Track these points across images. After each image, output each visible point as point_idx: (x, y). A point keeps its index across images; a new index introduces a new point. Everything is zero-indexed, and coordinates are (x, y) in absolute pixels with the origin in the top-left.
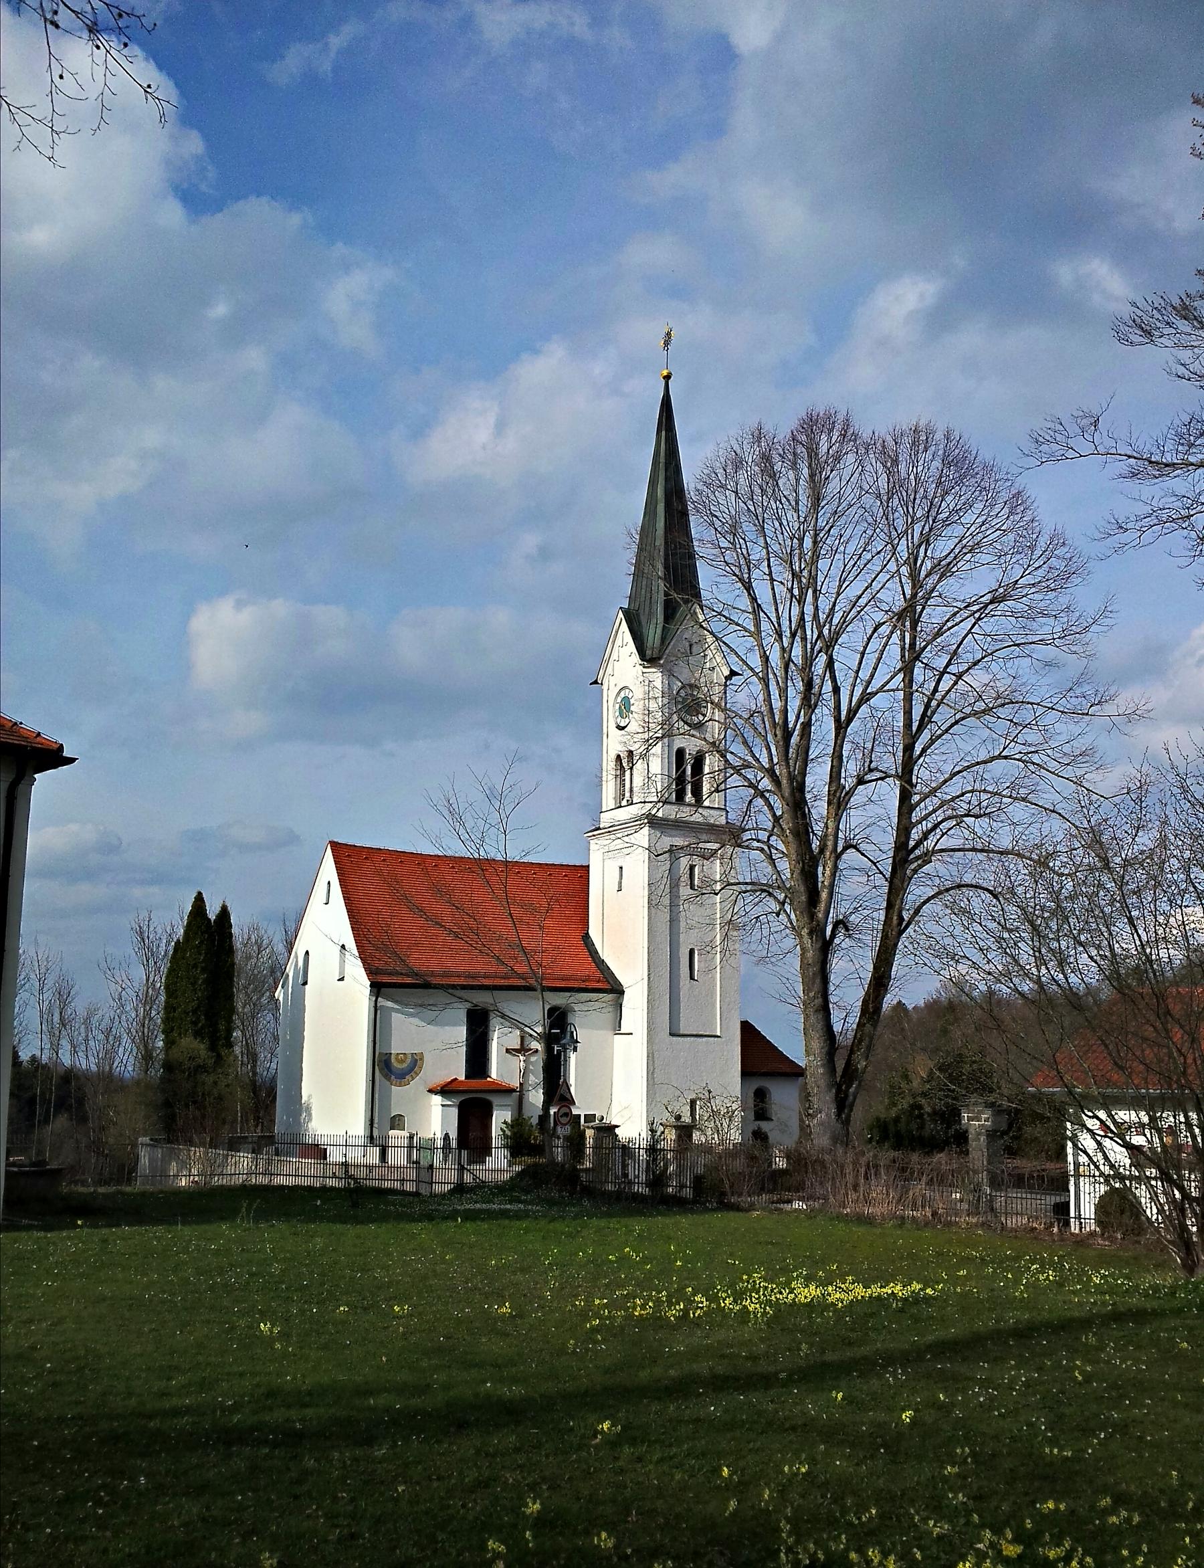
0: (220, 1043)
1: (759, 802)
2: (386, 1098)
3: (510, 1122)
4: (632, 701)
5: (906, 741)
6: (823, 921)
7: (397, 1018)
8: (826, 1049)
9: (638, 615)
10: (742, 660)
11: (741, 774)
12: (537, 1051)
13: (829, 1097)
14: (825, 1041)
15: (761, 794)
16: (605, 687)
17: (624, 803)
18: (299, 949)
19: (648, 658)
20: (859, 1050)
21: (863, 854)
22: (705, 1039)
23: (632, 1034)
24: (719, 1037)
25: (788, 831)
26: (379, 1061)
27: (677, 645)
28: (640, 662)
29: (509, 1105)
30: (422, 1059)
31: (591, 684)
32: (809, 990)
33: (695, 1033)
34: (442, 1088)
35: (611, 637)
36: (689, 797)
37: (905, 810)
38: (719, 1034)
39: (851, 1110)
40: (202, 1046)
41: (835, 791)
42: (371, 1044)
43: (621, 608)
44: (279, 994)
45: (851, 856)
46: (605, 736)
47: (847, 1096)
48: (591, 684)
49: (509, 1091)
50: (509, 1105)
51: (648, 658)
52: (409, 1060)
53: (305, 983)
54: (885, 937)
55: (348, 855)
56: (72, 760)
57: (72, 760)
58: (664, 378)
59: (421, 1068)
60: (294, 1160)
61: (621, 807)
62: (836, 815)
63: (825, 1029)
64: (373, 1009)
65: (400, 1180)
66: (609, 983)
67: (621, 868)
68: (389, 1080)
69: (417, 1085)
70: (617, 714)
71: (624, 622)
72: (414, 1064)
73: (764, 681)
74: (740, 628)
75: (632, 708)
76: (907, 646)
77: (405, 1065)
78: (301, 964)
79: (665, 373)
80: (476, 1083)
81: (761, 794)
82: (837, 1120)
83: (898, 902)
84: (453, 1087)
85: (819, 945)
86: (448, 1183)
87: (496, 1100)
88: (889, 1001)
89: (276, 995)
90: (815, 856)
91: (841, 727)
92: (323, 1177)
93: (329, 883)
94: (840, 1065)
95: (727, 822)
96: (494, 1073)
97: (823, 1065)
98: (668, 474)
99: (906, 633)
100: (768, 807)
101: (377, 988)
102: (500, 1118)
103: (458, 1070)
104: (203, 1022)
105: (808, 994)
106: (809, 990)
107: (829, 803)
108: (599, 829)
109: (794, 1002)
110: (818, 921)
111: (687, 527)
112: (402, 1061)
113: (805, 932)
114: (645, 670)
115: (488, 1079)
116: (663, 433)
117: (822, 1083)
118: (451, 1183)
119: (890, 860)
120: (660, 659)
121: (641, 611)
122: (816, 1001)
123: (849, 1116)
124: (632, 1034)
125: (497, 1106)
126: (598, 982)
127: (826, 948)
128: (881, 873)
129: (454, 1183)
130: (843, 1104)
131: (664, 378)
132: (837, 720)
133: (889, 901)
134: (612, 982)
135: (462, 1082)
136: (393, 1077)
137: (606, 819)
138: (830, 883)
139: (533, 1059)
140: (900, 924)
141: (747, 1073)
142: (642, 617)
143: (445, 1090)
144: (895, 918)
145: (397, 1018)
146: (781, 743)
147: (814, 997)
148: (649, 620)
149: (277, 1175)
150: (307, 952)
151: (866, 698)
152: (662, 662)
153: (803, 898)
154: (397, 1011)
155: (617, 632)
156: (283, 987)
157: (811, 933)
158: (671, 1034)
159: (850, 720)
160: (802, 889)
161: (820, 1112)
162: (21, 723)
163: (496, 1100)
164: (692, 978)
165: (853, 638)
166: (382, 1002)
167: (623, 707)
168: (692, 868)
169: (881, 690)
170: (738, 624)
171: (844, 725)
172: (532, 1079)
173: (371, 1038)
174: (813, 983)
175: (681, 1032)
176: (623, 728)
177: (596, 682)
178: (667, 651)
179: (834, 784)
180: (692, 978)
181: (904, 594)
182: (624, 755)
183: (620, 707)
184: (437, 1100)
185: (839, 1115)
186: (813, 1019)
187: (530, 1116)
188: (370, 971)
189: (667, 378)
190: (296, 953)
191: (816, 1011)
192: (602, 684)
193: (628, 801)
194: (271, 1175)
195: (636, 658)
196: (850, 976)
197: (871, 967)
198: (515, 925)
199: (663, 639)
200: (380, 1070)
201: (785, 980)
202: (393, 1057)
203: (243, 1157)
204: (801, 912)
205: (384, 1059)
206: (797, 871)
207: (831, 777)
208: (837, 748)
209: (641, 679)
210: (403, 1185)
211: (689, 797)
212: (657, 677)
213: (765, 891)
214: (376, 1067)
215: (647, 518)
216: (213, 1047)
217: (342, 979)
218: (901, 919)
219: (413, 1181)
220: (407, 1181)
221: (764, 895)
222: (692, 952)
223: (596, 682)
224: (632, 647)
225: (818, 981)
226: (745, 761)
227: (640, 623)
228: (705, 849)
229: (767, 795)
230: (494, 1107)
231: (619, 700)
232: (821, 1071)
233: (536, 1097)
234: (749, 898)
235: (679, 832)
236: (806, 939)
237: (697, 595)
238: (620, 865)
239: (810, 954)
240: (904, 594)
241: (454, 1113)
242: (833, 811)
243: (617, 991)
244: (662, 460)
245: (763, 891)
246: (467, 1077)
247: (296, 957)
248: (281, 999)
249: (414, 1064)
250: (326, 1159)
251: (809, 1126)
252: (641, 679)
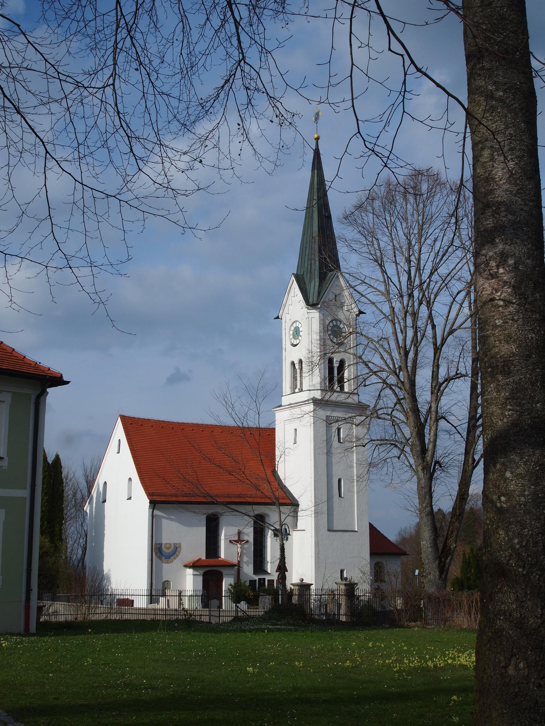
0: (56, 538)
1: (388, 391)
2: (160, 570)
3: (233, 584)
4: (301, 329)
5: (474, 357)
6: (430, 462)
7: (165, 522)
8: (433, 537)
9: (303, 278)
10: (379, 310)
11: (378, 376)
12: (248, 541)
13: (435, 565)
14: (432, 532)
15: (390, 386)
16: (283, 321)
17: (297, 390)
18: (100, 480)
19: (311, 304)
20: (451, 537)
21: (448, 422)
22: (348, 533)
23: (305, 530)
24: (356, 531)
25: (409, 409)
26: (155, 548)
27: (329, 296)
28: (306, 306)
29: (232, 574)
30: (180, 547)
31: (275, 319)
32: (423, 503)
33: (343, 529)
34: (193, 564)
35: (284, 290)
36: (336, 387)
37: (474, 396)
38: (356, 530)
39: (447, 573)
40: (47, 540)
41: (435, 386)
42: (150, 538)
43: (293, 274)
44: (87, 508)
45: (442, 423)
46: (284, 351)
47: (445, 565)
48: (275, 319)
49: (232, 566)
50: (232, 574)
51: (311, 303)
52: (172, 548)
53: (104, 501)
54: (464, 471)
55: (152, 426)
56: (67, 383)
57: (67, 383)
58: (315, 139)
59: (180, 552)
60: (126, 608)
61: (294, 393)
62: (436, 400)
63: (432, 526)
64: (151, 517)
65: (199, 615)
66: (290, 500)
67: (296, 430)
68: (161, 559)
69: (177, 563)
70: (291, 337)
71: (295, 282)
72: (176, 550)
73: (392, 322)
74: (375, 290)
75: (301, 334)
76: (472, 301)
77: (170, 551)
78: (101, 489)
79: (316, 136)
80: (212, 561)
81: (390, 386)
82: (439, 578)
83: (472, 450)
84: (198, 564)
85: (428, 476)
86: (229, 616)
87: (224, 571)
88: (467, 507)
89: (85, 509)
90: (423, 424)
91: (437, 350)
92: (154, 614)
93: (119, 440)
94: (441, 546)
95: (359, 402)
96: (222, 556)
97: (431, 547)
98: (319, 195)
99: (471, 293)
100: (394, 395)
101: (154, 504)
102: (227, 583)
103: (201, 554)
104: (46, 525)
105: (422, 505)
106: (423, 503)
107: (432, 393)
108: (281, 406)
109: (412, 509)
110: (427, 462)
111: (331, 226)
112: (168, 548)
113: (420, 468)
114: (309, 311)
115: (219, 559)
116: (316, 171)
117: (431, 557)
118: (231, 616)
119: (466, 425)
120: (318, 304)
121: (305, 276)
122: (427, 509)
123: (446, 576)
124: (305, 530)
125: (226, 575)
126: (283, 499)
127: (431, 477)
128: (459, 433)
129: (233, 616)
130: (443, 569)
131: (315, 139)
132: (435, 344)
133: (466, 449)
134: (291, 499)
135: (204, 560)
136: (163, 558)
137: (285, 401)
138: (434, 440)
139: (246, 546)
140: (473, 463)
141: (373, 553)
142: (305, 279)
143: (195, 565)
144: (470, 459)
145: (165, 522)
146: (403, 358)
147: (426, 506)
148: (310, 281)
149: (126, 613)
150: (105, 483)
151: (451, 332)
152: (319, 306)
153: (418, 449)
154: (164, 518)
155: (290, 288)
156: (89, 503)
157: (423, 469)
158: (329, 530)
159: (442, 344)
160: (418, 443)
161: (430, 574)
162: (40, 363)
163: (224, 571)
164: (340, 496)
165: (444, 298)
166: (156, 512)
167: (295, 333)
168: (339, 429)
169: (459, 327)
170: (373, 287)
171: (440, 347)
172: (245, 559)
173: (150, 534)
174: (425, 498)
175: (335, 529)
176: (295, 345)
177: (278, 318)
178: (322, 300)
179: (435, 382)
180: (340, 496)
181: (470, 271)
182: (296, 362)
183: (293, 333)
184: (190, 571)
185: (440, 576)
186: (425, 519)
187: (245, 581)
188: (149, 495)
189: (317, 139)
190: (98, 483)
191: (427, 515)
192: (281, 319)
193: (299, 389)
194: (122, 613)
195: (303, 303)
196: (445, 494)
197: (457, 488)
198: (264, 468)
199: (319, 292)
200: (156, 554)
201: (406, 497)
202: (163, 546)
203: (101, 607)
204: (418, 457)
205: (157, 547)
206: (414, 433)
207: (432, 378)
208: (436, 361)
209: (307, 316)
210: (201, 618)
211: (336, 387)
212: (315, 314)
213: (392, 444)
214: (153, 551)
215: (307, 220)
216: (52, 541)
217: (130, 498)
218: (474, 460)
219: (207, 615)
220: (203, 615)
221: (392, 446)
222: (340, 481)
223: (278, 318)
224: (300, 296)
225: (427, 497)
226: (381, 368)
227: (305, 283)
228: (334, 417)
229: (393, 387)
230: (224, 576)
231: (293, 328)
232: (430, 550)
233: (248, 570)
234: (382, 449)
235: (341, 409)
236: (421, 473)
237: (338, 267)
238: (295, 428)
239: (423, 482)
240: (470, 271)
241: (200, 579)
242: (434, 398)
243: (294, 504)
244: (316, 187)
245: (392, 444)
246: (206, 558)
247: (99, 486)
248: (88, 511)
249: (176, 550)
250: (133, 606)
251: (423, 582)
252: (307, 316)
